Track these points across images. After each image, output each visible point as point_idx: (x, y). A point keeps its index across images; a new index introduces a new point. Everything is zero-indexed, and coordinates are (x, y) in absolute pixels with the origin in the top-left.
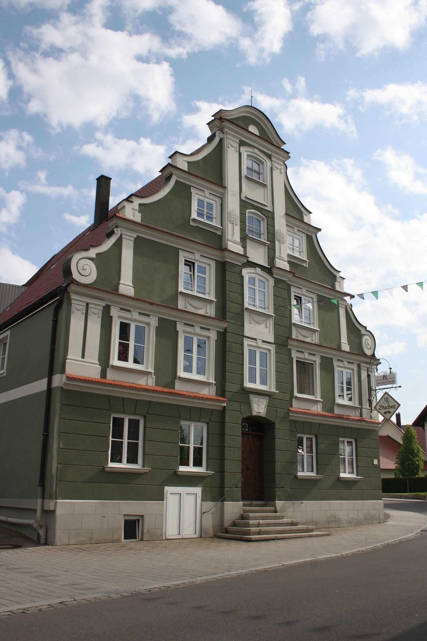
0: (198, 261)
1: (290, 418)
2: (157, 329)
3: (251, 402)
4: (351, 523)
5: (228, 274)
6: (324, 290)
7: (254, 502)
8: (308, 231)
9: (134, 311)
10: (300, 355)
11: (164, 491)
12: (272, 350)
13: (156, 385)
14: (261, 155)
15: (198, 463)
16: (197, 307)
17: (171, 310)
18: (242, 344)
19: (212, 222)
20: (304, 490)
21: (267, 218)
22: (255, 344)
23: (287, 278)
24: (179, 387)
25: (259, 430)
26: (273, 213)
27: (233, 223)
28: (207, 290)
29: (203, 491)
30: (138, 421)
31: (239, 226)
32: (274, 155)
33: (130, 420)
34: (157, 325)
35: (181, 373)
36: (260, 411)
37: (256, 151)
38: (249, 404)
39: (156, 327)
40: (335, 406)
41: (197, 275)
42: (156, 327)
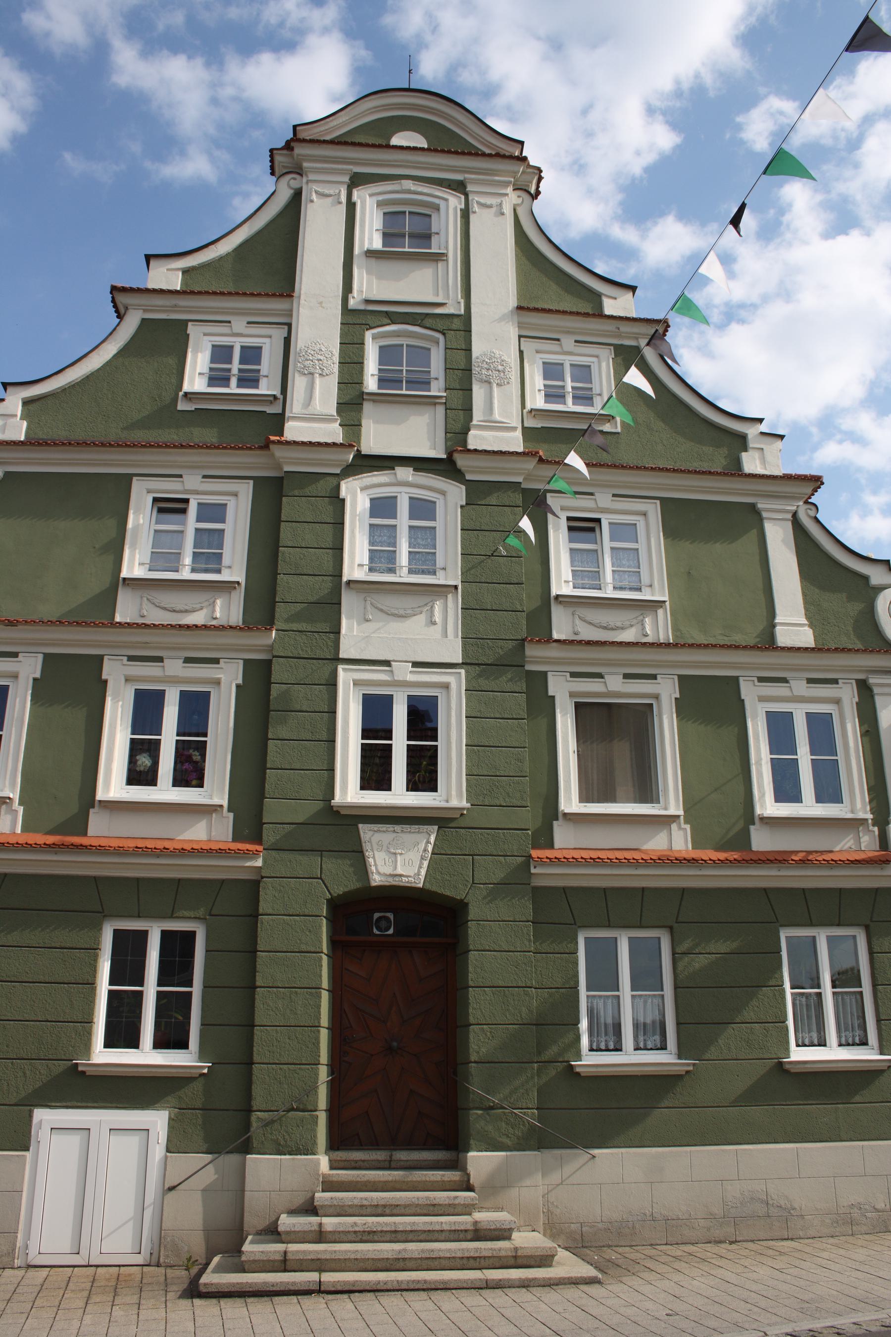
0: (197, 492)
1: (536, 882)
2: (680, 704)
3: (366, 847)
5: (292, 506)
6: (696, 483)
7: (402, 1155)
8: (619, 336)
9: (795, 679)
11: (31, 1126)
12: (454, 686)
13: (694, 847)
14: (426, 190)
15: (171, 1037)
16: (179, 607)
17: (644, 649)
18: (332, 684)
19: (593, 406)
20: (616, 1111)
21: (444, 334)
23: (519, 474)
24: (761, 841)
26: (467, 318)
27: (312, 374)
28: (645, 579)
29: (173, 1125)
30: (192, 935)
31: (334, 380)
32: (473, 176)
33: (165, 934)
34: (678, 696)
35: (767, 805)
36: (399, 871)
37: (408, 184)
38: (357, 855)
39: (676, 699)
40: (752, 828)
41: (612, 548)
42: (676, 699)
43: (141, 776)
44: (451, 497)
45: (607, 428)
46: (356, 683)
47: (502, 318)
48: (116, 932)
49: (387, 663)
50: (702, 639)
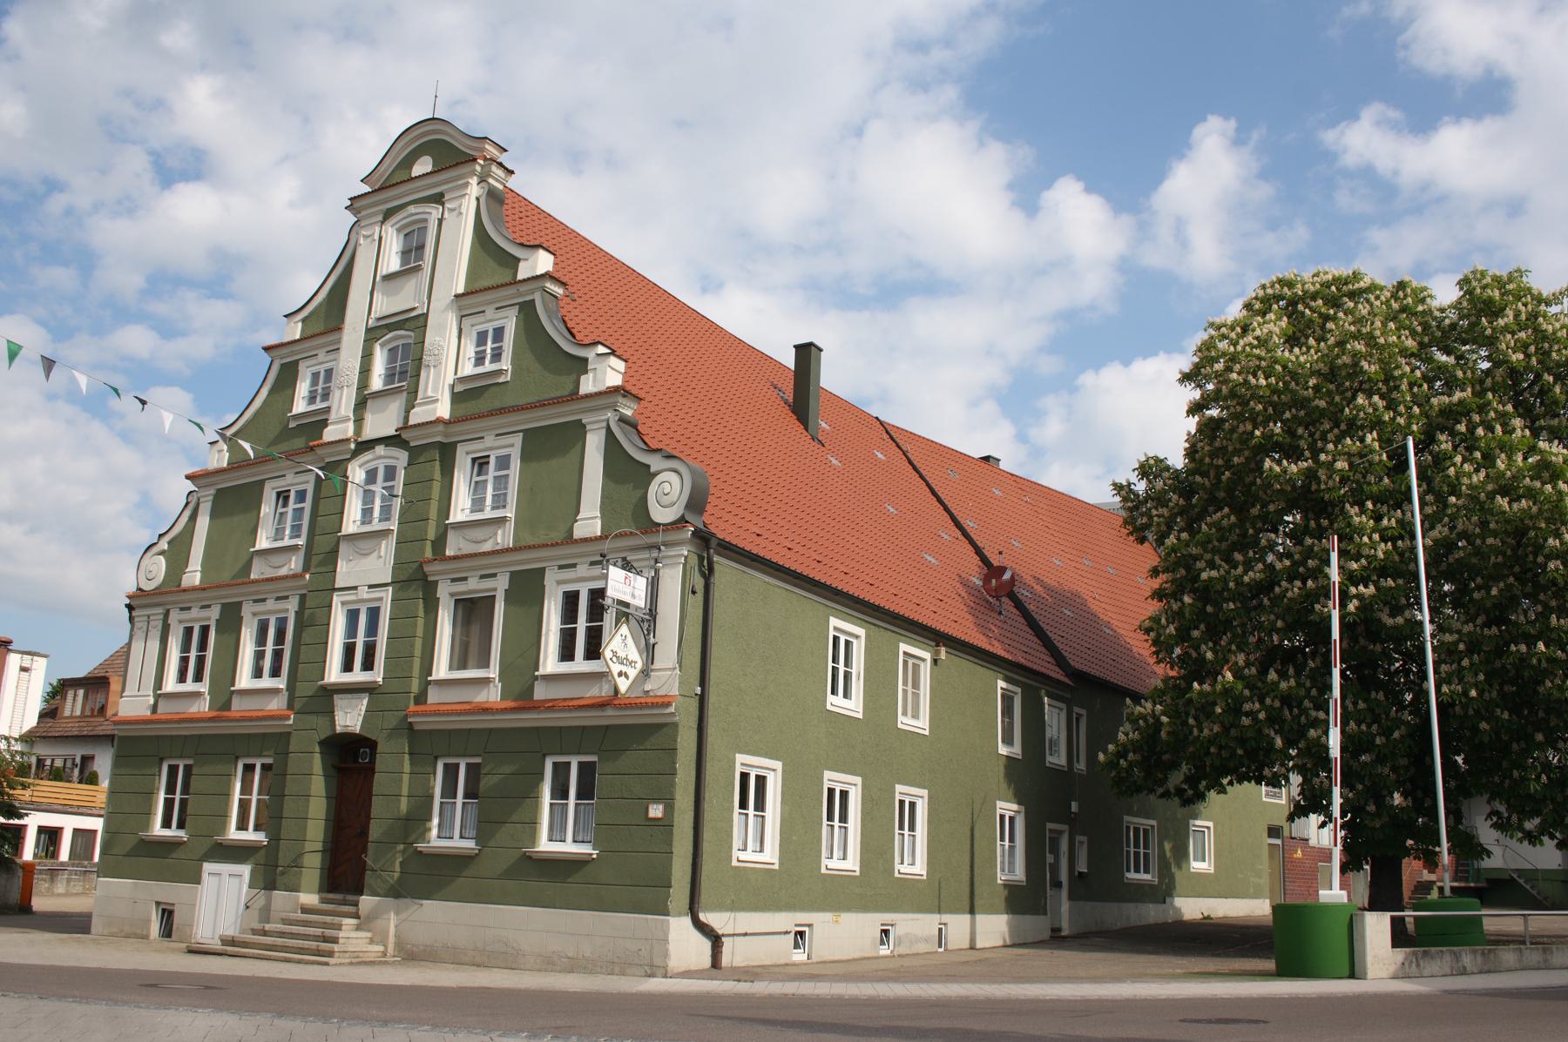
0: (491, 449)
4: (554, 964)
8: (522, 295)
10: (460, 587)
20: (435, 877)
22: (353, 598)
24: (541, 692)
25: (350, 759)
33: (581, 764)
38: (330, 713)
43: (567, 654)
44: (401, 458)
45: (501, 380)
46: (343, 603)
47: (446, 309)
48: (555, 764)
49: (355, 588)
50: (535, 541)
